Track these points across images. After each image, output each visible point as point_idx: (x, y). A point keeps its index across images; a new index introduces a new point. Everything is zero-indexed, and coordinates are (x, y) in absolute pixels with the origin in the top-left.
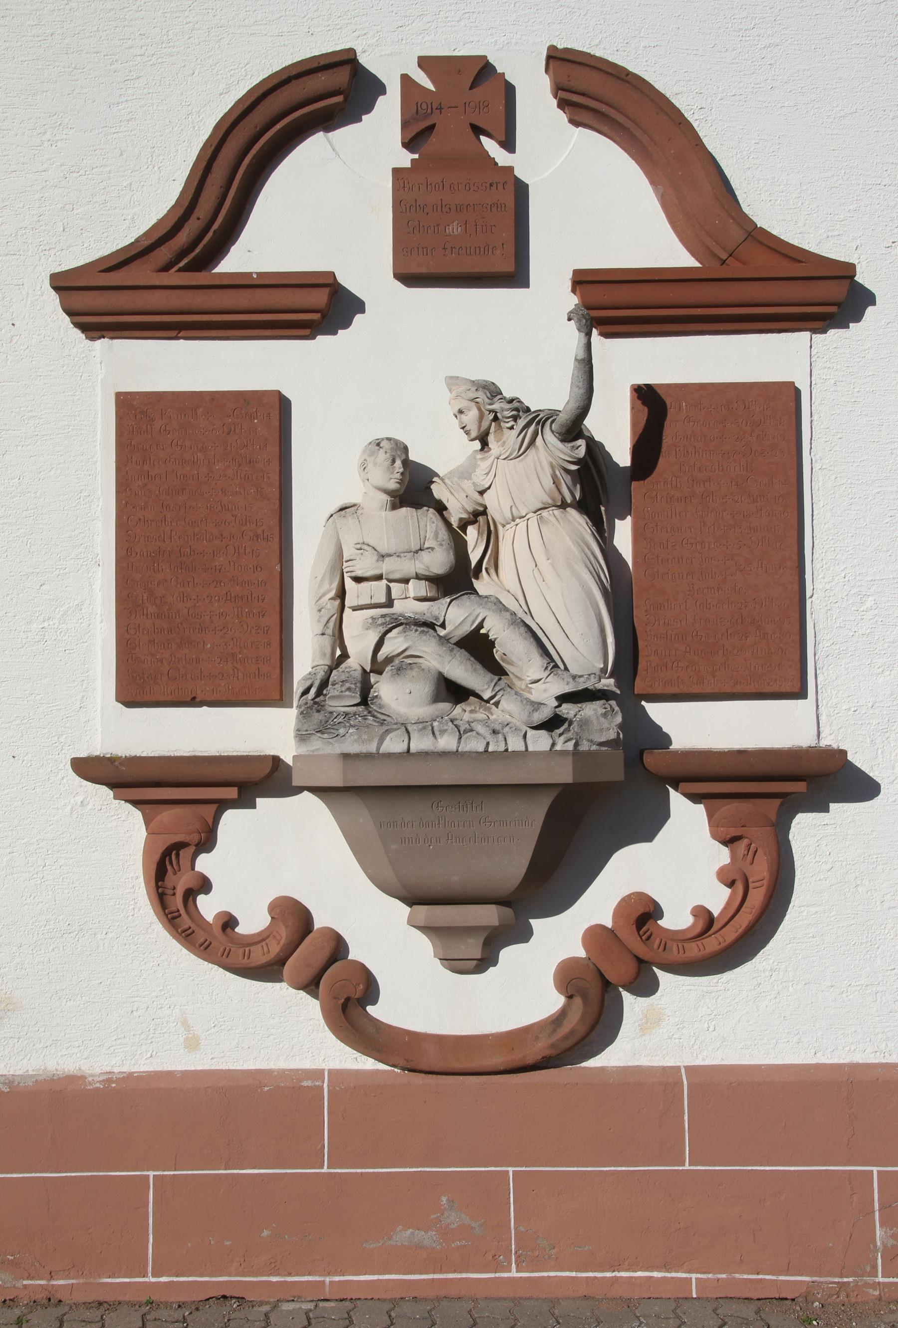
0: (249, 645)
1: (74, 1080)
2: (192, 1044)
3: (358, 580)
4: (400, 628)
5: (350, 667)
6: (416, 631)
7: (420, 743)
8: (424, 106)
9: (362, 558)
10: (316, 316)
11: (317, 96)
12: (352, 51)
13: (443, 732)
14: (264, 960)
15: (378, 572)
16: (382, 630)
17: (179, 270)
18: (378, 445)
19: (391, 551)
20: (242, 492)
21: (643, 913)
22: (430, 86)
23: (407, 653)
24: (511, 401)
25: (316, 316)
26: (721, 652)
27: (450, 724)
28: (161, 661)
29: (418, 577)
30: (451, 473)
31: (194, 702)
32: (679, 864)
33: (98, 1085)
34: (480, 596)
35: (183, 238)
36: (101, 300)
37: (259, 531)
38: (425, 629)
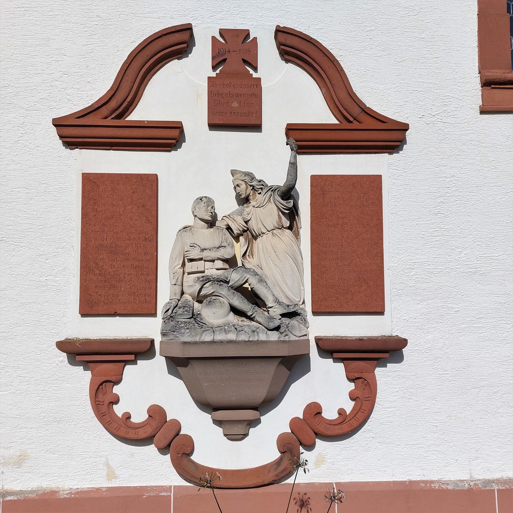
1: (54, 492)
2: (111, 475)
3: (191, 260)
4: (210, 283)
7: (220, 337)
8: (222, 50)
10: (173, 141)
11: (172, 44)
12: (190, 24)
14: (144, 436)
16: (202, 283)
17: (112, 119)
18: (201, 199)
21: (314, 411)
22: (224, 42)
23: (214, 294)
24: (260, 181)
25: (173, 141)
28: (100, 295)
29: (219, 259)
30: (232, 213)
31: (115, 315)
32: (325, 385)
33: (65, 496)
35: (113, 104)
36: (75, 132)
37: (147, 237)
38: (222, 283)
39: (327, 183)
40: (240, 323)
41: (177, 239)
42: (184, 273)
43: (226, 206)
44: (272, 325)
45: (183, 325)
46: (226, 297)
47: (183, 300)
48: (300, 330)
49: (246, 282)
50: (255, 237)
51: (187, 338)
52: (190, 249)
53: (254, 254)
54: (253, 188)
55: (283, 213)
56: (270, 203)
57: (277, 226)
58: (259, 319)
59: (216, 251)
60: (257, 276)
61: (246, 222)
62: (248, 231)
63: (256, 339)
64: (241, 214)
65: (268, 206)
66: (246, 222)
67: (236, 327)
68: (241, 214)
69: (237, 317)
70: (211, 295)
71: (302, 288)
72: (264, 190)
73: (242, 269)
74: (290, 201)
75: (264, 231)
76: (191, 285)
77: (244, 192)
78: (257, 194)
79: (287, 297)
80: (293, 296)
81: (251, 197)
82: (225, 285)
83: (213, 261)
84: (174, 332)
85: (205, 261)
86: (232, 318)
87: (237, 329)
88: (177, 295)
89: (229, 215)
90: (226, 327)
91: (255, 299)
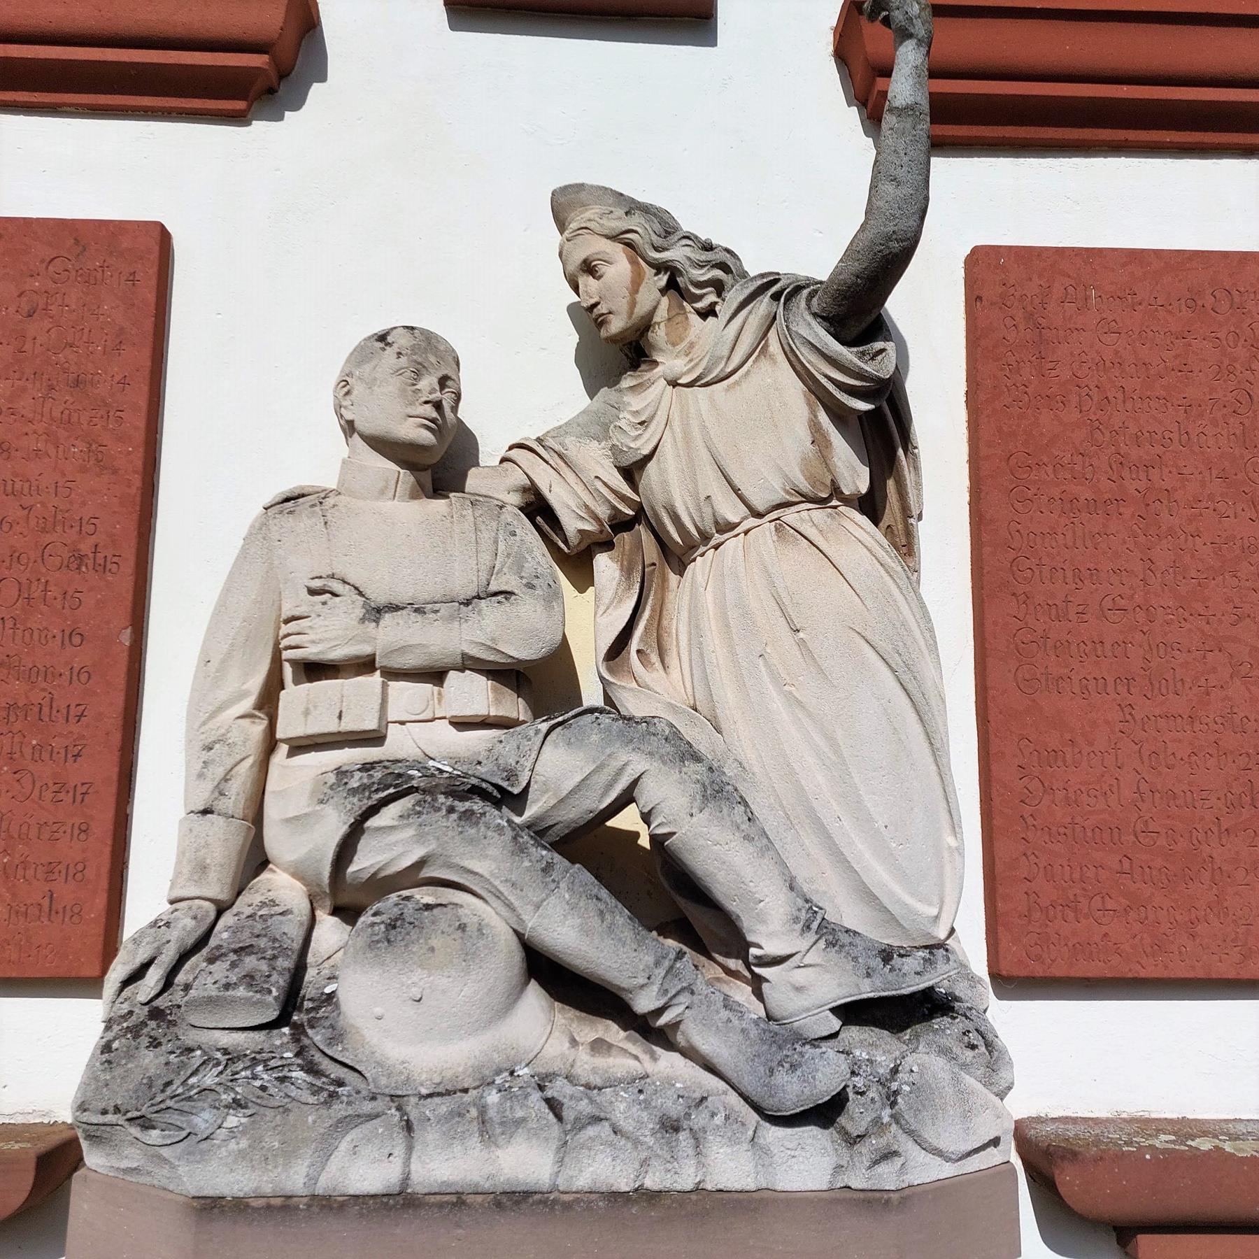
0: (34, 832)
3: (314, 670)
5: (273, 903)
6: (451, 810)
7: (445, 1164)
9: (326, 609)
13: (514, 1125)
15: (366, 649)
16: (358, 804)
19: (401, 597)
20: (52, 451)
23: (427, 873)
26: (1206, 875)
27: (536, 1096)
29: (468, 664)
34: (629, 719)
37: (85, 547)
38: (477, 805)
39: (1057, 291)
40: (587, 1064)
41: (244, 554)
42: (271, 744)
43: (522, 391)
44: (794, 1091)
45: (209, 1078)
46: (499, 896)
47: (245, 904)
48: (966, 1115)
49: (627, 798)
50: (677, 556)
51: (225, 1175)
52: (306, 603)
53: (670, 644)
54: (672, 285)
55: (839, 415)
56: (764, 364)
57: (805, 487)
58: (707, 1044)
59: (451, 618)
60: (691, 767)
61: (631, 473)
62: (641, 529)
63: (685, 1179)
64: (599, 427)
65: (755, 379)
66: (631, 473)
67: (559, 1089)
68: (599, 427)
69: (565, 1017)
70: (412, 876)
71: (951, 841)
72: (728, 295)
73: (605, 720)
74: (878, 345)
75: (731, 511)
76: (304, 822)
77: (621, 304)
78: (694, 319)
79: (868, 896)
80: (897, 889)
81: (659, 335)
82: (498, 817)
83: (435, 675)
84: (145, 1123)
85: (393, 674)
86: (540, 1029)
87: (560, 1107)
88: (213, 875)
89: (539, 440)
90: (493, 1097)
91: (673, 899)
